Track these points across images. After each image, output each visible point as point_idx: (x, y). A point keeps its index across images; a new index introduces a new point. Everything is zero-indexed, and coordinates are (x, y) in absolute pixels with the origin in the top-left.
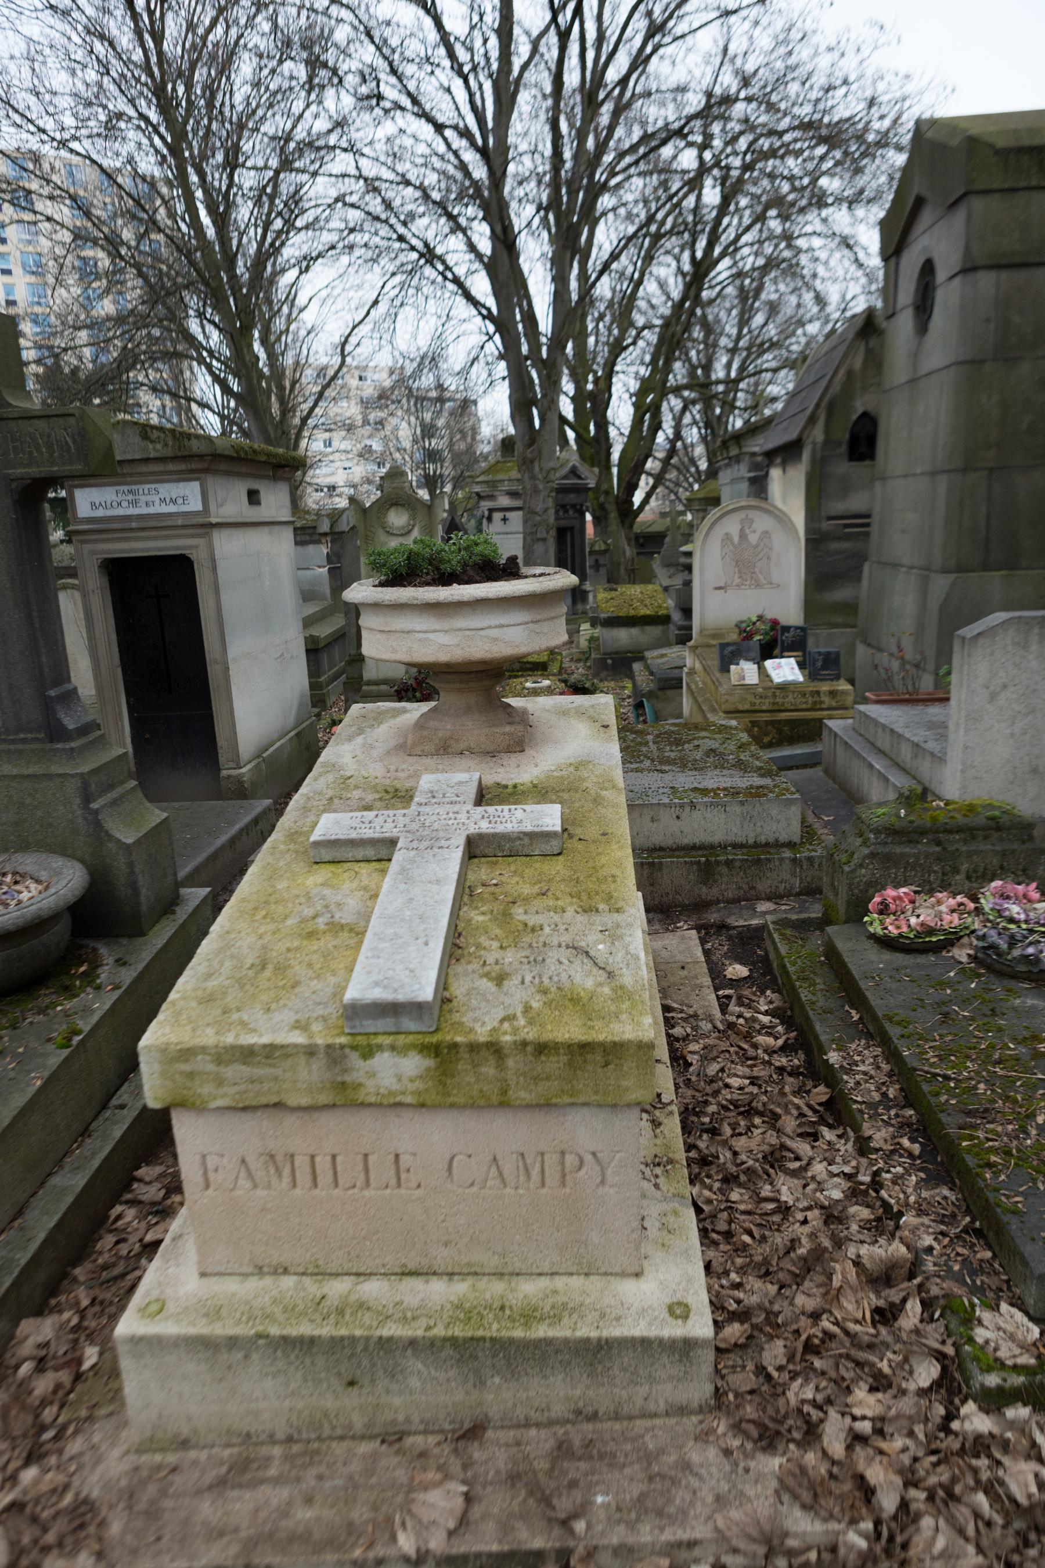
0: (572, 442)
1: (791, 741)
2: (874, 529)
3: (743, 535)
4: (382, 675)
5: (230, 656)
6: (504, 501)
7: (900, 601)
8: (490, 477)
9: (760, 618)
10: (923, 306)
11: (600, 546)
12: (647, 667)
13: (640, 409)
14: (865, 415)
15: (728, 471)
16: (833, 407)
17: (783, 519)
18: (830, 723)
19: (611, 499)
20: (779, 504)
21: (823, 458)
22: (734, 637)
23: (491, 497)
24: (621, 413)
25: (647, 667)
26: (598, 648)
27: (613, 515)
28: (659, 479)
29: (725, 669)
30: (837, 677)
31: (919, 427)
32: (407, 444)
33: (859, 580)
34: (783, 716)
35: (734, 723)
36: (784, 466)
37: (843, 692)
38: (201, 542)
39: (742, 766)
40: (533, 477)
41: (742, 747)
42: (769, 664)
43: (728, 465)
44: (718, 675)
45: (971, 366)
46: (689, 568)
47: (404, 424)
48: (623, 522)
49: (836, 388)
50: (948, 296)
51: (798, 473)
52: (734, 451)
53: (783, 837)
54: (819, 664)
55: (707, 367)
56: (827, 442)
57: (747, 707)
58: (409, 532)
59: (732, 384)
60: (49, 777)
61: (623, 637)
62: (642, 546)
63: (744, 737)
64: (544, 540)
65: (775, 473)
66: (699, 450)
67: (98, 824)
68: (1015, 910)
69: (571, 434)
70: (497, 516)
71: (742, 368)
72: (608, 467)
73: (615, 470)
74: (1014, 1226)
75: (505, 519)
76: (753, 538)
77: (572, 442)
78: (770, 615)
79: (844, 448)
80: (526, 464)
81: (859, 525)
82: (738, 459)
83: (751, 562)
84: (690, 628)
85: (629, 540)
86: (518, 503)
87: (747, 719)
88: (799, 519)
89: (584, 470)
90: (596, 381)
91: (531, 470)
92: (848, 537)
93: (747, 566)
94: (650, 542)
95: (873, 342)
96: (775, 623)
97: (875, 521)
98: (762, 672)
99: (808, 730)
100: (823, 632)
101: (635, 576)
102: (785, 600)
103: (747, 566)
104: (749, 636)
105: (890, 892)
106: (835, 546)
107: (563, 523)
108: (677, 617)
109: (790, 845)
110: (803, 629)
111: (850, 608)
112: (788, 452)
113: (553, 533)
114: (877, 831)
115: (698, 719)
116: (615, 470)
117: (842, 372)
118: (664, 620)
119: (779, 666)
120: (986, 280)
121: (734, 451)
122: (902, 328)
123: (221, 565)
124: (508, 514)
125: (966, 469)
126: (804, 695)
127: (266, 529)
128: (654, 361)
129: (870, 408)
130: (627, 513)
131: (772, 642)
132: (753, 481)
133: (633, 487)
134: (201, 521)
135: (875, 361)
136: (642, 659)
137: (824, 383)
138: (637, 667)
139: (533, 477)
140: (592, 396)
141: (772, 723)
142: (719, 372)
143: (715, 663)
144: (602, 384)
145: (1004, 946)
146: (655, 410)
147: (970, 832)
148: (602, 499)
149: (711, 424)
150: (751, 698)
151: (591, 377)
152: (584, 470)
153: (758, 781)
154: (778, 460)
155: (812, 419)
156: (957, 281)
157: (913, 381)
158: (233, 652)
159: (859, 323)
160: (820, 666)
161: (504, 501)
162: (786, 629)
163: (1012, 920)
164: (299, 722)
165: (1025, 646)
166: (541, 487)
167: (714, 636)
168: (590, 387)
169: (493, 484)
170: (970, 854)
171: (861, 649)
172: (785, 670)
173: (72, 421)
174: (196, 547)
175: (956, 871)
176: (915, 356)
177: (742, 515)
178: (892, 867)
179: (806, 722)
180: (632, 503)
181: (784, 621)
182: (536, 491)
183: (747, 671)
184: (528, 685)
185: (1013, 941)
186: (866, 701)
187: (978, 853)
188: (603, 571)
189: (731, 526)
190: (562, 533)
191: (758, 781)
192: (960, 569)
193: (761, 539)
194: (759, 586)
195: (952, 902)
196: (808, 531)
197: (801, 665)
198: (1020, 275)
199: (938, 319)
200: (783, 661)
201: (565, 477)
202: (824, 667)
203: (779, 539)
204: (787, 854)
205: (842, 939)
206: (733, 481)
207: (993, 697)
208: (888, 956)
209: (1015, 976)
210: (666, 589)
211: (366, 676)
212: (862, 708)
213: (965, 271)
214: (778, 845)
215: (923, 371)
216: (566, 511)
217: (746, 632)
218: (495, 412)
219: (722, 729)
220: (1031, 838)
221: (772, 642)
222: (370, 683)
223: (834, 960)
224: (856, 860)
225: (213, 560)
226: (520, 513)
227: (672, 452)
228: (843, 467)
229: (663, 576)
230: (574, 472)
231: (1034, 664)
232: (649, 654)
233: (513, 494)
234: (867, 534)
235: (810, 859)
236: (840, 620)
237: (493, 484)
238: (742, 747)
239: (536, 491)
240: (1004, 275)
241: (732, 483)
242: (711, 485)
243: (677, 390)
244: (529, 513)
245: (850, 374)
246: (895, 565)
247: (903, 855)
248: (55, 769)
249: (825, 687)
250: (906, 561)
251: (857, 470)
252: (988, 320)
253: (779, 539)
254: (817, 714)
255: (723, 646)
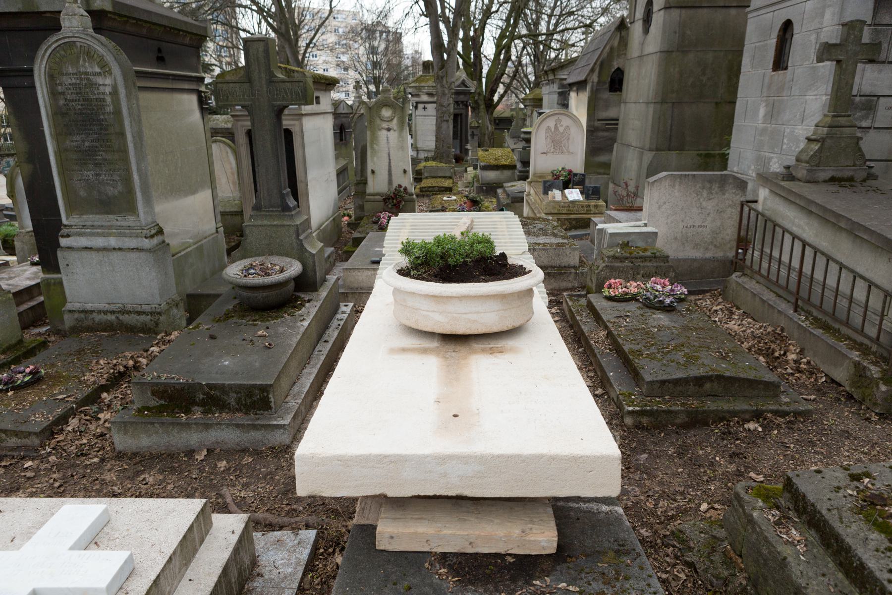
0: (461, 67)
1: (576, 228)
2: (620, 127)
3: (556, 127)
4: (376, 191)
5: (309, 178)
6: (425, 98)
7: (630, 160)
8: (417, 84)
9: (563, 169)
10: (647, 20)
11: (475, 124)
12: (505, 191)
13: (499, 47)
14: (618, 69)
15: (548, 87)
16: (602, 64)
17: (576, 120)
18: (594, 219)
19: (482, 98)
20: (575, 113)
21: (597, 89)
22: (550, 178)
23: (418, 95)
24: (489, 49)
25: (505, 191)
26: (478, 181)
27: (482, 107)
28: (508, 87)
29: (546, 192)
30: (599, 199)
31: (643, 78)
32: (364, 59)
33: (612, 151)
34: (572, 216)
35: (550, 218)
36: (577, 92)
37: (601, 206)
38: (297, 123)
39: (555, 235)
40: (443, 86)
41: (554, 228)
42: (566, 191)
43: (547, 84)
44: (542, 196)
45: (667, 54)
46: (528, 141)
47: (362, 48)
48: (487, 111)
49: (605, 55)
50: (658, 18)
51: (584, 97)
52: (551, 77)
53: (572, 264)
54: (590, 192)
55: (537, 23)
56: (599, 82)
57: (556, 211)
58: (392, 120)
59: (549, 34)
60: (283, 226)
61: (492, 175)
62: (498, 124)
63: (555, 224)
64: (447, 121)
65: (573, 95)
66: (530, 69)
67: (302, 246)
68: (659, 287)
69: (461, 61)
70: (421, 106)
71: (556, 25)
72: (481, 81)
73: (484, 80)
74: (642, 371)
75: (425, 108)
76: (561, 129)
77: (461, 67)
78: (567, 168)
79: (607, 85)
80: (439, 79)
81: (613, 124)
82: (553, 82)
83: (559, 138)
84: (528, 172)
85: (490, 121)
86: (431, 99)
87: (556, 217)
88: (584, 120)
89: (469, 82)
90: (475, 31)
91: (441, 82)
92: (608, 130)
93: (558, 143)
94: (503, 123)
95: (623, 33)
96: (570, 171)
97: (620, 122)
98: (563, 195)
99: (585, 224)
100: (594, 177)
101: (498, 143)
102: (576, 162)
103: (558, 143)
104: (558, 177)
105: (613, 281)
106: (601, 134)
107: (457, 111)
108: (519, 165)
109: (574, 267)
110: (583, 175)
111: (607, 165)
112: (580, 85)
113: (452, 117)
114: (608, 257)
115: (531, 215)
116: (484, 80)
117: (608, 47)
118: (512, 167)
119: (572, 193)
120: (675, 13)
121: (551, 77)
122: (637, 29)
123: (306, 134)
124: (427, 105)
125: (663, 102)
126: (583, 207)
127: (322, 116)
128: (507, 20)
129: (621, 66)
130: (490, 106)
131: (569, 181)
132: (560, 94)
133: (493, 91)
134: (297, 112)
135: (624, 43)
136: (502, 187)
137: (599, 52)
138: (499, 191)
139: (443, 86)
140: (474, 39)
141: (567, 219)
142: (543, 27)
143: (541, 189)
144: (479, 32)
145: (652, 298)
146: (508, 48)
147: (644, 259)
148: (476, 98)
149: (538, 58)
150: (558, 207)
151: (472, 29)
152: (469, 82)
153: (561, 241)
154: (575, 88)
155: (592, 70)
156: (662, 12)
157: (640, 57)
158: (310, 177)
159: (617, 23)
160: (591, 193)
161: (425, 98)
162: (576, 175)
163: (657, 291)
164: (334, 213)
165: (674, 186)
166: (447, 92)
167: (540, 177)
168: (472, 33)
169: (419, 88)
170: (644, 267)
171: (611, 185)
172: (574, 194)
173: (301, 84)
174: (294, 125)
175: (638, 274)
176: (642, 44)
177: (556, 117)
178: (613, 271)
179: (584, 219)
180: (493, 100)
181: (575, 171)
182: (444, 94)
183: (556, 194)
184: (445, 198)
185: (656, 297)
186: (611, 209)
187: (647, 266)
188: (476, 138)
189: (551, 122)
190: (456, 116)
191: (561, 241)
192: (657, 150)
193: (565, 130)
194: (563, 153)
195: (636, 284)
196: (588, 126)
197: (582, 193)
198: (691, 12)
199: (652, 28)
200: (573, 190)
201: (459, 86)
202: (593, 194)
203: (574, 130)
204: (573, 271)
205: (592, 297)
206: (550, 93)
207: (660, 207)
208: (610, 303)
209: (656, 309)
210: (513, 150)
211: (368, 191)
212: (608, 212)
213: (665, 8)
214: (569, 267)
215: (646, 53)
216: (458, 105)
217: (556, 176)
218: (418, 42)
219: (544, 220)
220: (668, 262)
221: (569, 181)
222: (369, 195)
223: (591, 307)
224: (600, 268)
225: (302, 132)
226: (435, 105)
227: (516, 72)
228: (606, 95)
229: (510, 142)
230: (463, 83)
231: (677, 194)
232: (505, 185)
233: (430, 94)
234: (617, 129)
235: (582, 273)
236: (602, 171)
237: (419, 88)
238: (554, 228)
239: (444, 94)
240: (684, 11)
241: (549, 94)
242: (537, 91)
243: (520, 37)
244: (440, 106)
245: (612, 48)
246: (629, 146)
247: (618, 267)
248: (285, 223)
249: (592, 203)
250: (634, 144)
251: (613, 96)
252: (675, 32)
253: (574, 130)
254: (588, 216)
255: (545, 182)
